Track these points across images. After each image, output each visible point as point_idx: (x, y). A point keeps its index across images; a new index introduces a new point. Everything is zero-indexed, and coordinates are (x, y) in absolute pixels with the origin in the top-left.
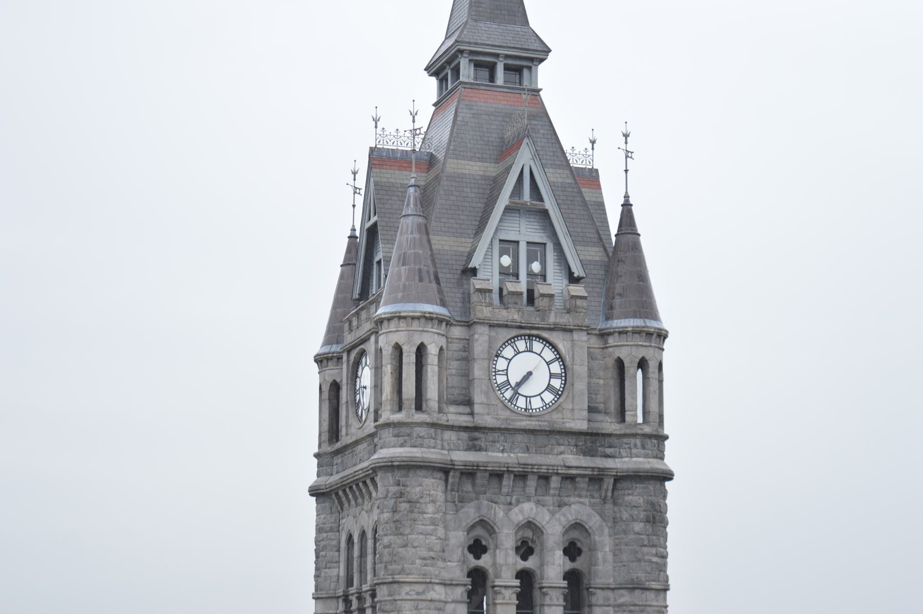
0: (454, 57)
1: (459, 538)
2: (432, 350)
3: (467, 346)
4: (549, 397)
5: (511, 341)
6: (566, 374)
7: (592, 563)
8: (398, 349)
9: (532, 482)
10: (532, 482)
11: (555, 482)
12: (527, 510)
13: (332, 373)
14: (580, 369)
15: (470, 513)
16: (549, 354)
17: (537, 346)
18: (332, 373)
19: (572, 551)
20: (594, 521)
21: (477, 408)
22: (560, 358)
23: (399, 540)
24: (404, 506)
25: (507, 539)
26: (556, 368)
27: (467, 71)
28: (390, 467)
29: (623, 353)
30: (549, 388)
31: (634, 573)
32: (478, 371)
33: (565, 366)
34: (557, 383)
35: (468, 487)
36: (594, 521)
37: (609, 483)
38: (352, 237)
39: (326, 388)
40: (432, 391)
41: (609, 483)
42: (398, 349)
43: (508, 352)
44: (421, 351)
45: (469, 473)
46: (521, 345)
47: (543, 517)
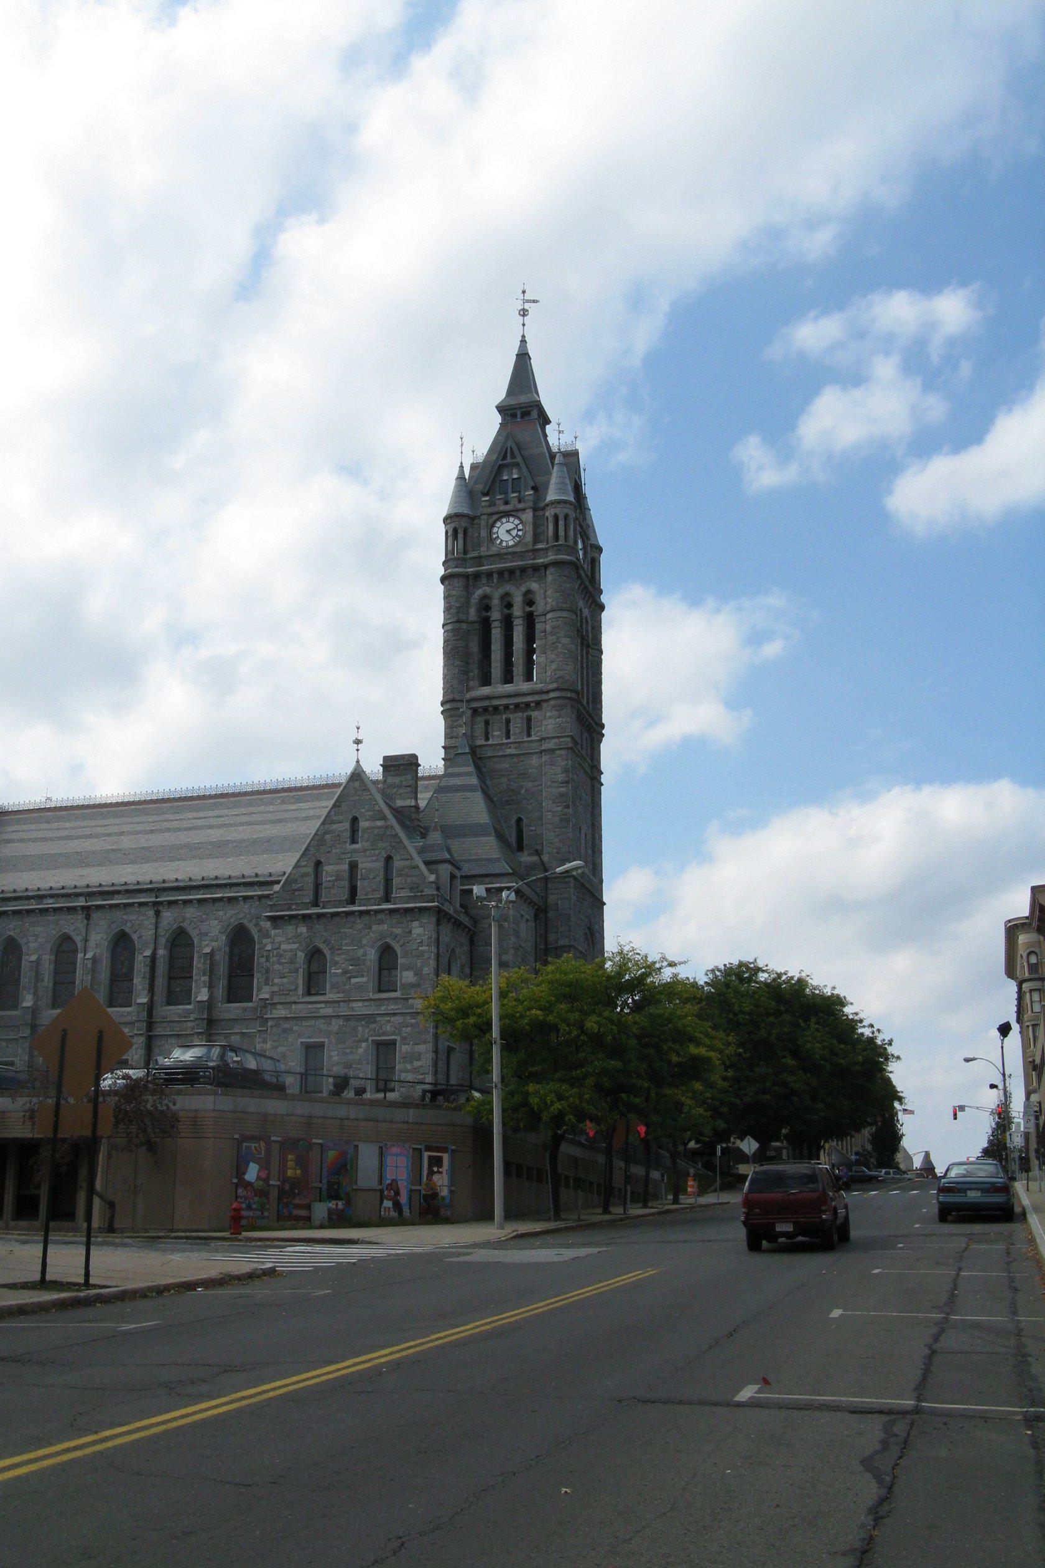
44: (566, 517)
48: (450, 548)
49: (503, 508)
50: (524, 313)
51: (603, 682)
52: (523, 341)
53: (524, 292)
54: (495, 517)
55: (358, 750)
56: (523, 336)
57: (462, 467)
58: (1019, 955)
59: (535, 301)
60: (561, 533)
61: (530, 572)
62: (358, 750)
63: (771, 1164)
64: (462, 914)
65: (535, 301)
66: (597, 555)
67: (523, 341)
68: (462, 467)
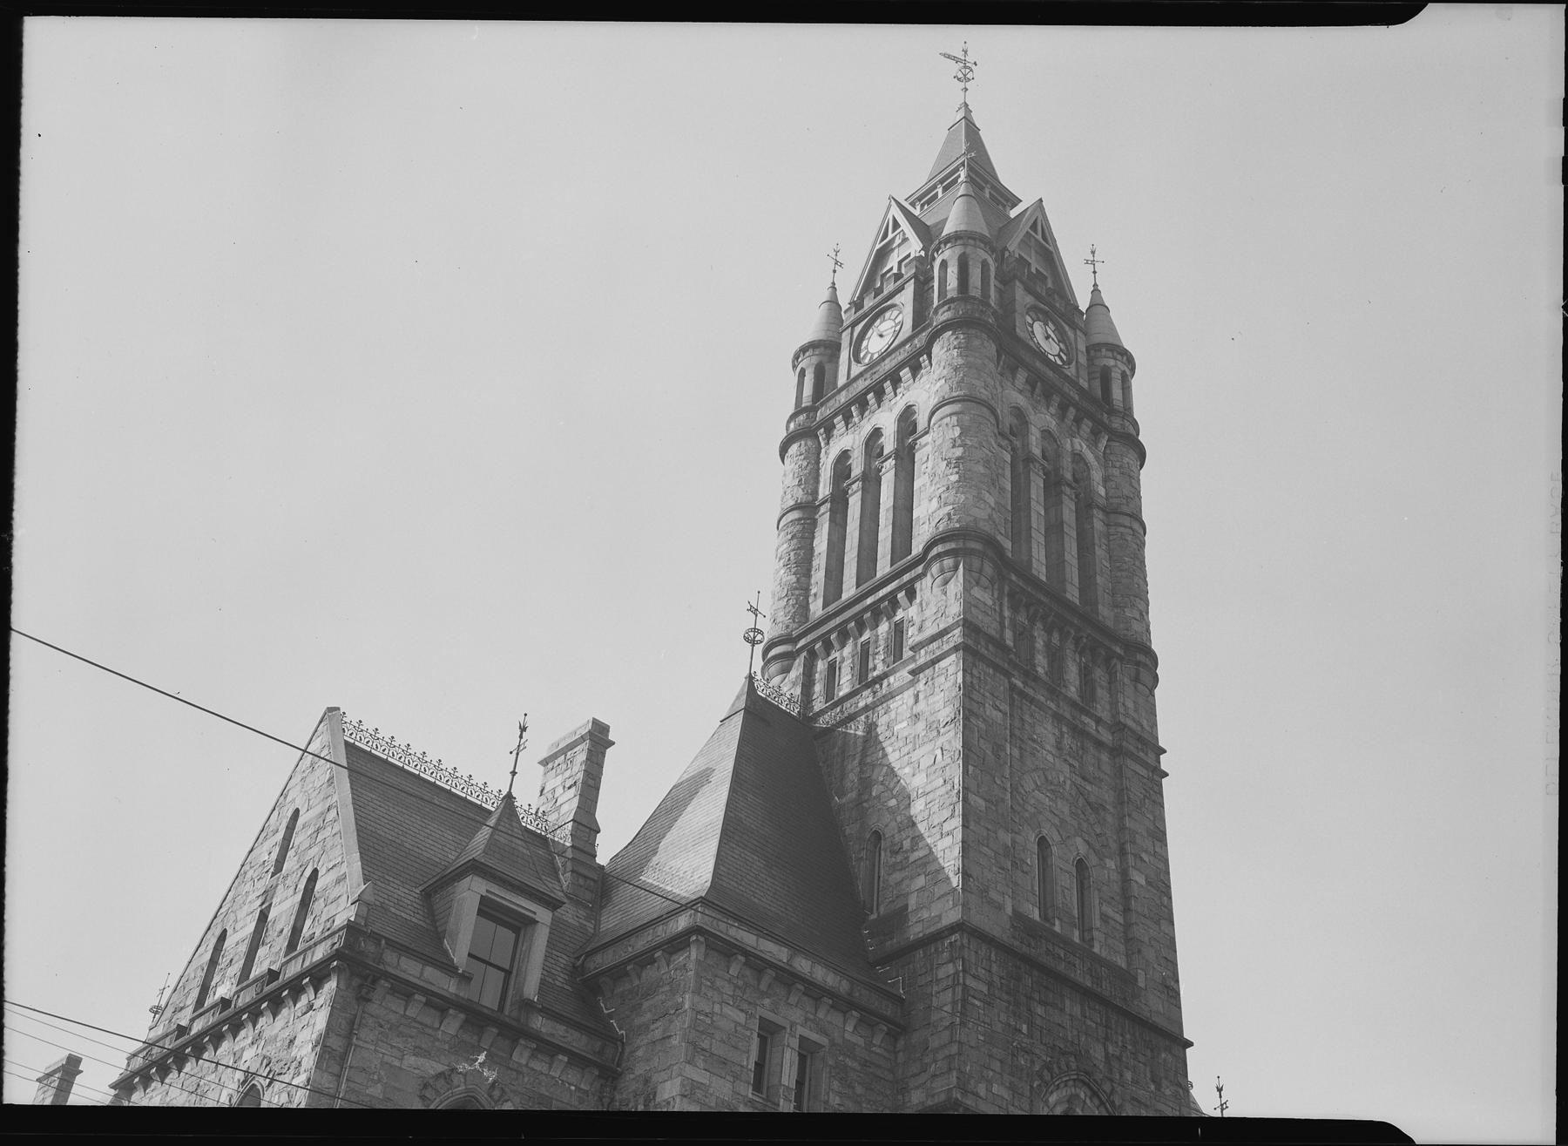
38: (833, 302)
61: (905, 373)
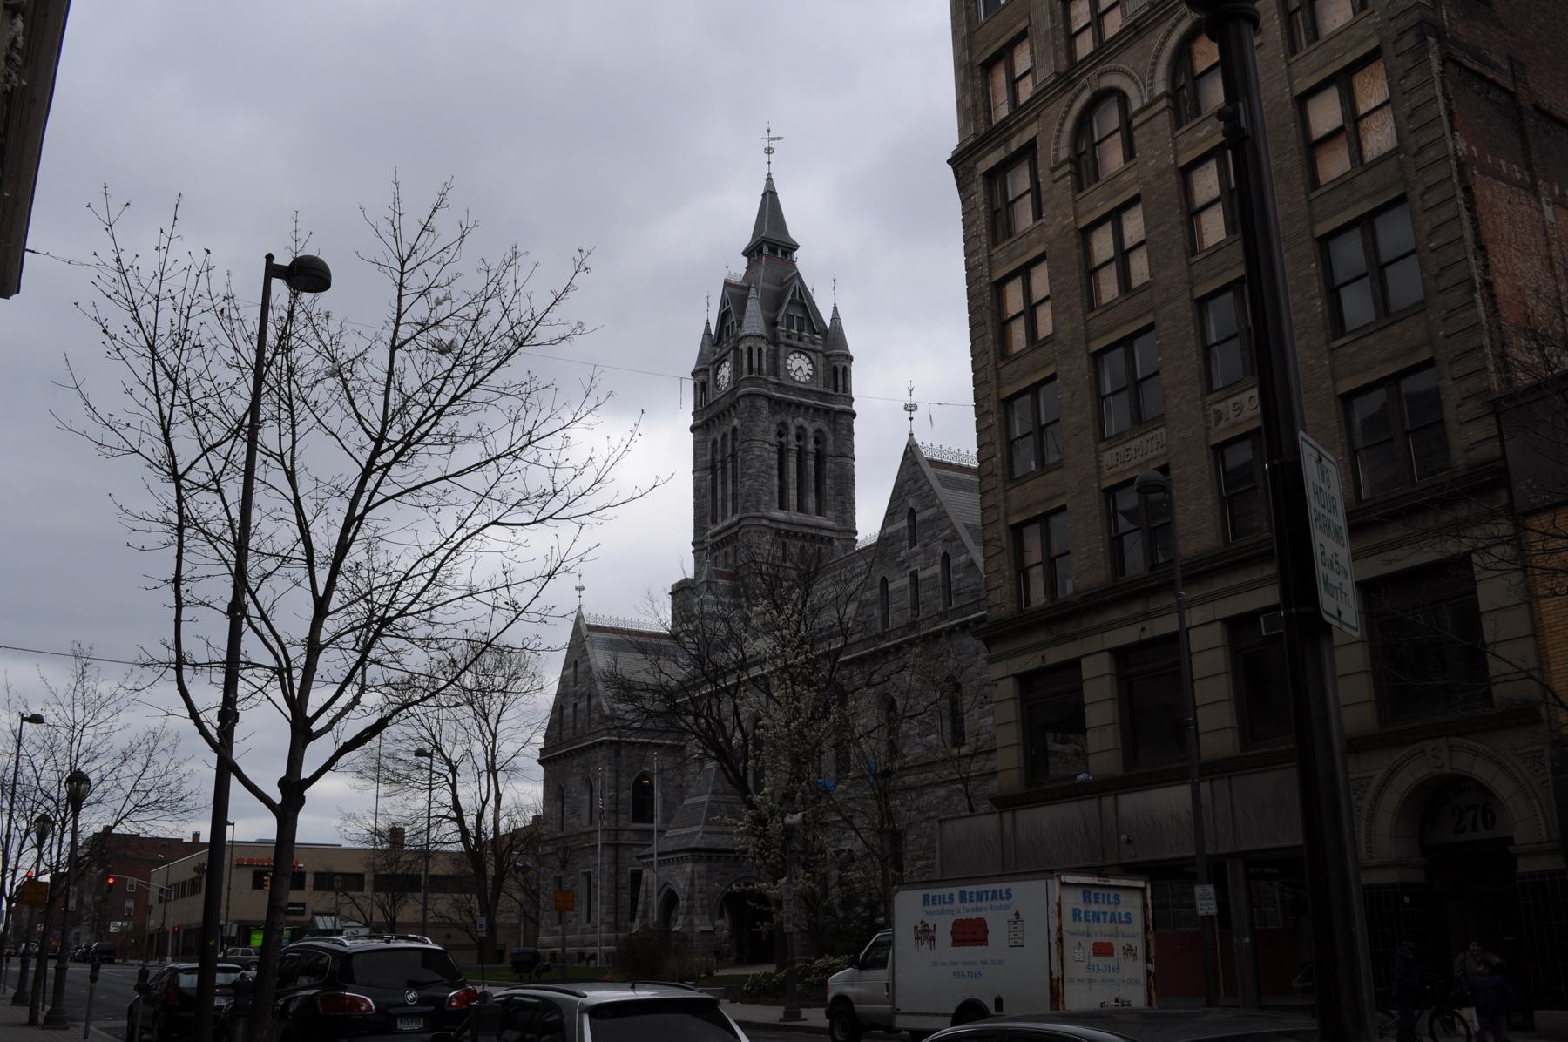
0: (761, 244)
1: (774, 427)
2: (764, 350)
3: (776, 351)
4: (808, 377)
5: (793, 353)
6: (815, 369)
7: (825, 446)
8: (750, 349)
9: (802, 410)
10: (802, 410)
11: (811, 411)
12: (800, 421)
13: (701, 377)
14: (821, 368)
15: (778, 418)
16: (807, 361)
17: (803, 357)
18: (701, 377)
19: (817, 441)
20: (826, 429)
21: (781, 377)
22: (812, 362)
23: (751, 424)
24: (754, 410)
25: (793, 431)
26: (810, 366)
27: (765, 250)
28: (749, 394)
29: (837, 364)
30: (808, 374)
31: (1354, 119)
32: (781, 362)
33: (814, 366)
34: (811, 373)
35: (777, 408)
36: (826, 429)
37: (832, 414)
38: (707, 332)
39: (699, 386)
40: (764, 367)
41: (832, 414)
42: (750, 349)
43: (792, 357)
44: (760, 349)
45: (778, 402)
46: (797, 355)
47: (806, 424)
48: (699, 399)
49: (795, 342)
50: (769, 151)
51: (857, 479)
52: (769, 179)
53: (769, 131)
54: (716, 366)
55: (911, 419)
56: (769, 174)
57: (708, 324)
58: (1318, 546)
59: (779, 139)
60: (755, 364)
62: (911, 419)
63: (1072, 638)
64: (814, 599)
65: (779, 139)
66: (847, 364)
67: (769, 179)
68: (708, 324)
